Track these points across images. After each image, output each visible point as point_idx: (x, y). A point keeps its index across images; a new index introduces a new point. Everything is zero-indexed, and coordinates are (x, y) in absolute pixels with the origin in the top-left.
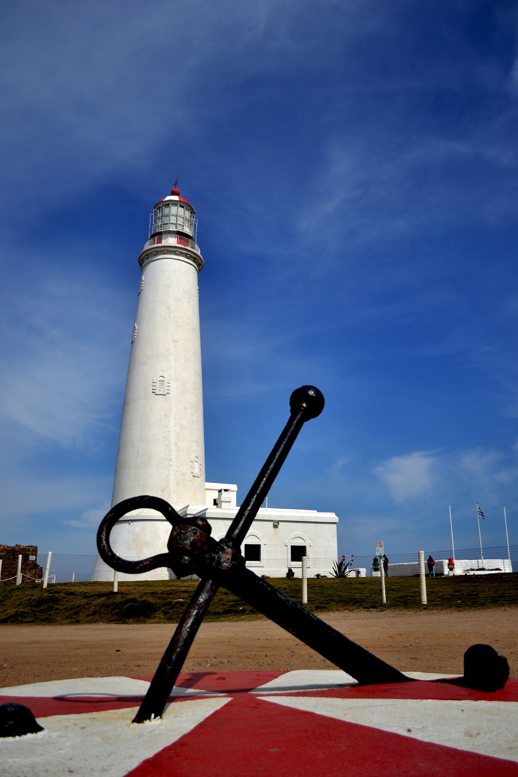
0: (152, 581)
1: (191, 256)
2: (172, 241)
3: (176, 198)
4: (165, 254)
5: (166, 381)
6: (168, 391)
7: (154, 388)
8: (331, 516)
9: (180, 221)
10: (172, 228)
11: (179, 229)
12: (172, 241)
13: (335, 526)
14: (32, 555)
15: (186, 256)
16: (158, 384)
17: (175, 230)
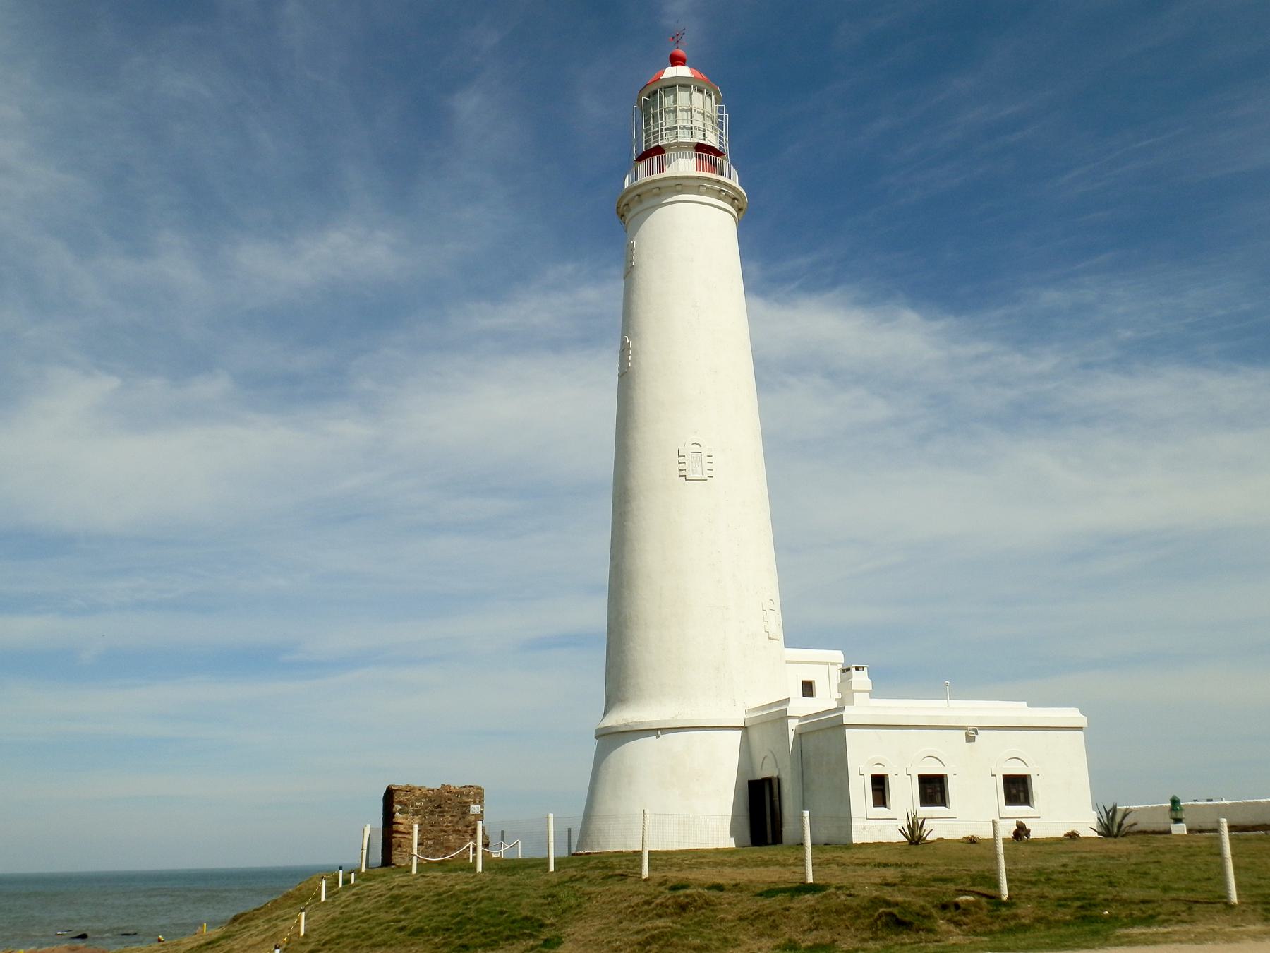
0: (681, 852)
1: (727, 194)
2: (684, 166)
3: (683, 71)
4: (699, 193)
5: (705, 454)
6: (710, 473)
7: (682, 466)
8: (1072, 716)
9: (698, 121)
10: (684, 137)
11: (698, 138)
12: (684, 166)
13: (1081, 733)
14: (475, 803)
15: (718, 194)
16: (689, 459)
17: (688, 140)
